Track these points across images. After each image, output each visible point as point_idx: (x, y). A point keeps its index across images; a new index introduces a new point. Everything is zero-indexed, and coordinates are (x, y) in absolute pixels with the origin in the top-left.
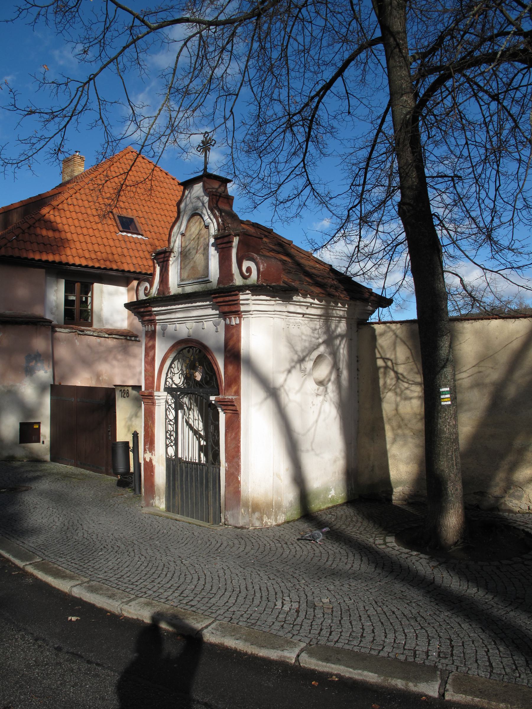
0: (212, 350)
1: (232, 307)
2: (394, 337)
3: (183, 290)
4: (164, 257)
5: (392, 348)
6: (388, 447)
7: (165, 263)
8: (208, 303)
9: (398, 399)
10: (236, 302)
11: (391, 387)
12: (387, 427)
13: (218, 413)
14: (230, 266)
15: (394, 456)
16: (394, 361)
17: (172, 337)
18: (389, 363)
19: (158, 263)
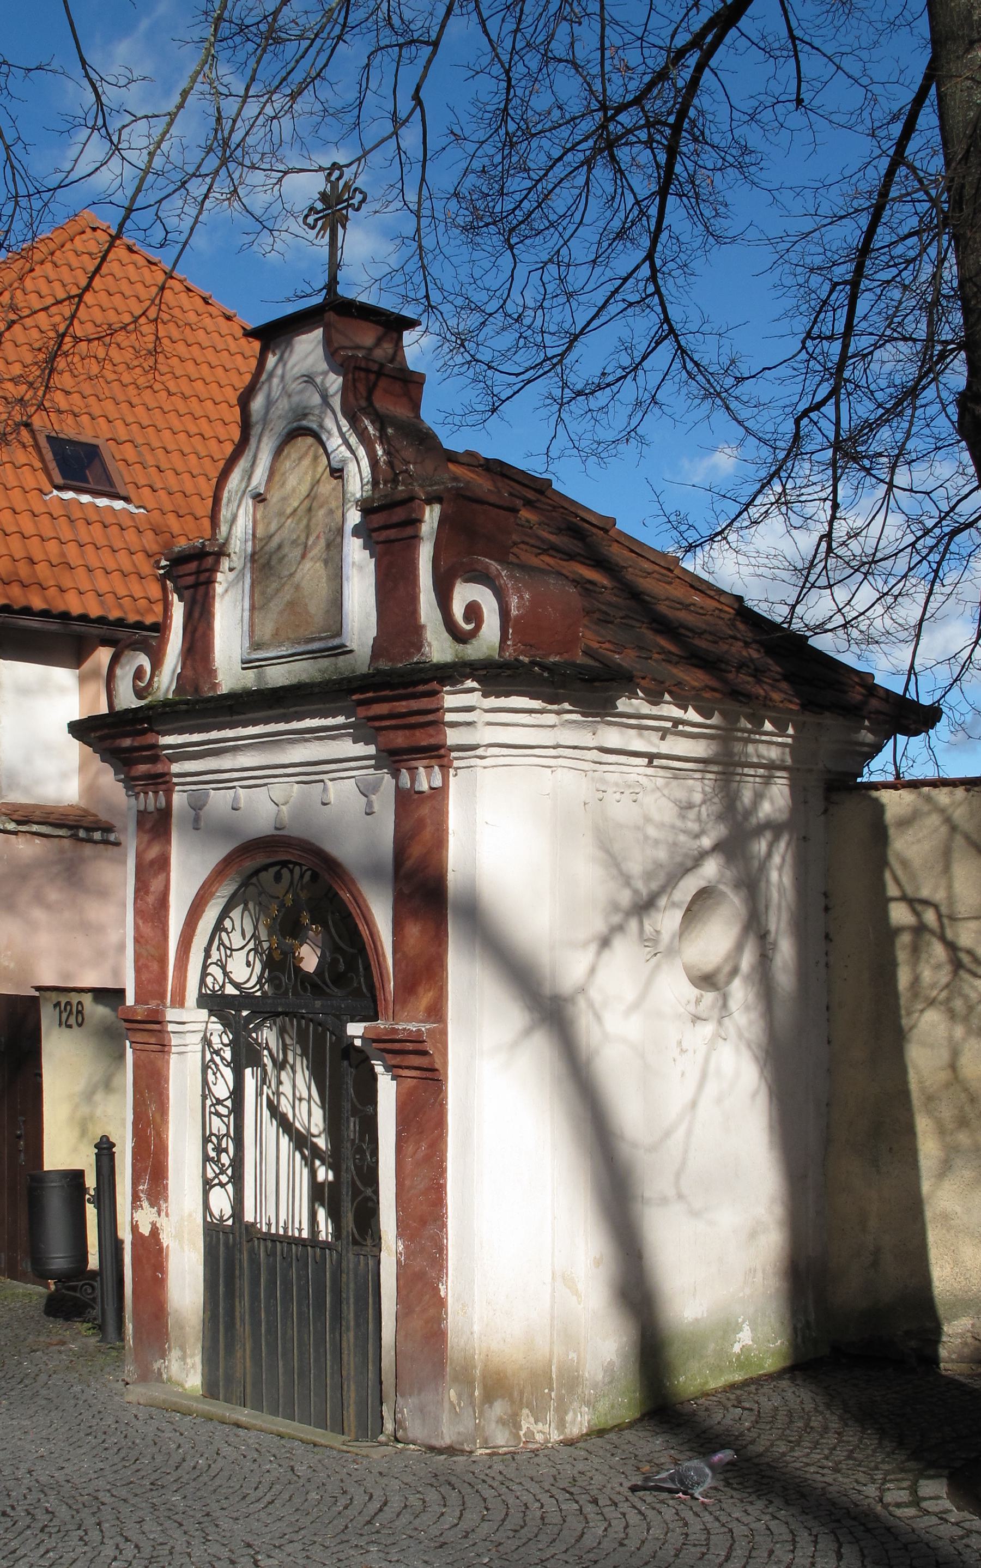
0: (354, 872)
1: (418, 733)
2: (944, 830)
3: (260, 677)
4: (198, 572)
5: (939, 868)
6: (926, 1186)
7: (202, 589)
8: (341, 720)
9: (959, 1031)
10: (430, 718)
11: (934, 993)
12: (923, 1124)
13: (374, 1078)
15: (945, 1217)
16: (944, 910)
17: (224, 830)
18: (930, 917)
19: (177, 590)
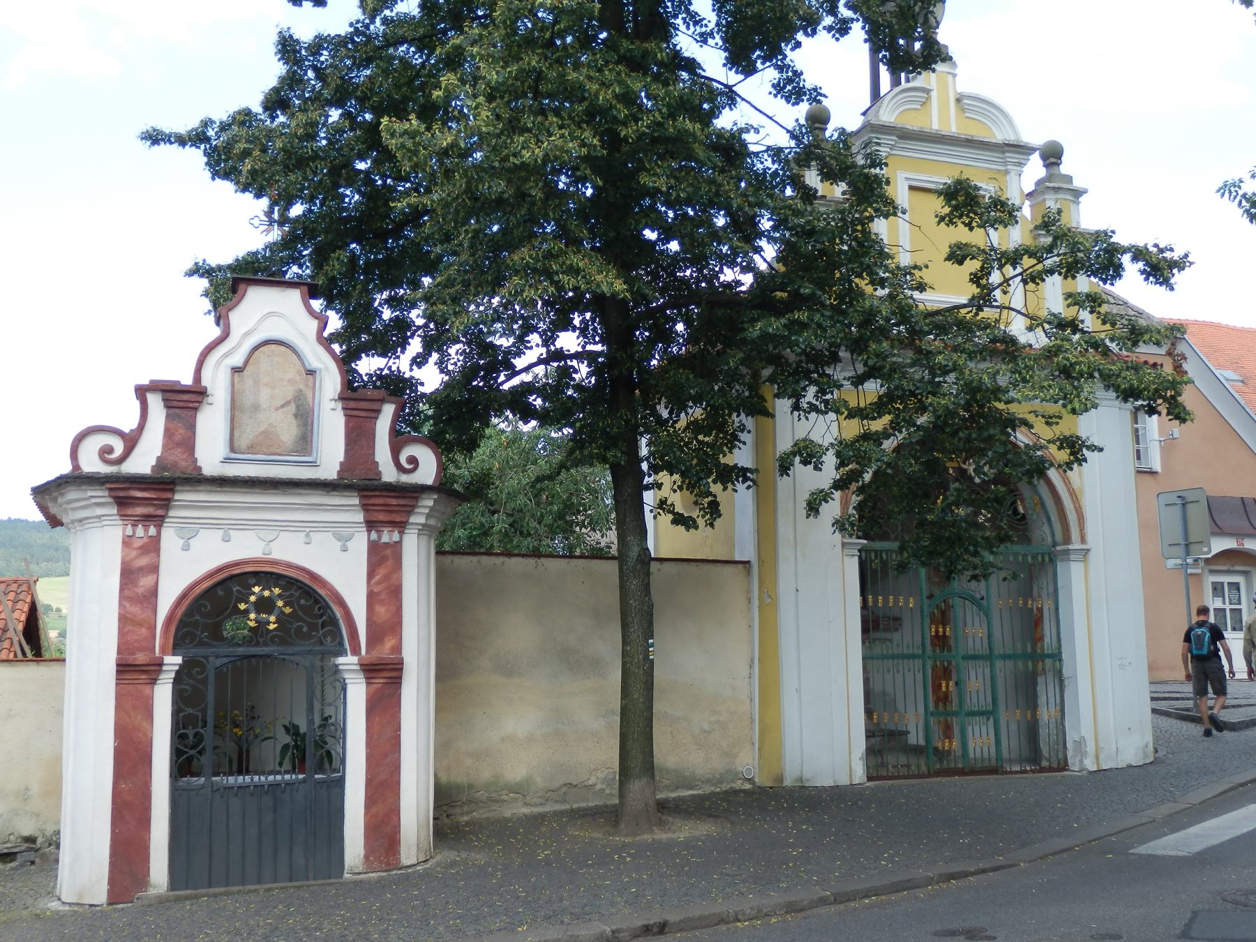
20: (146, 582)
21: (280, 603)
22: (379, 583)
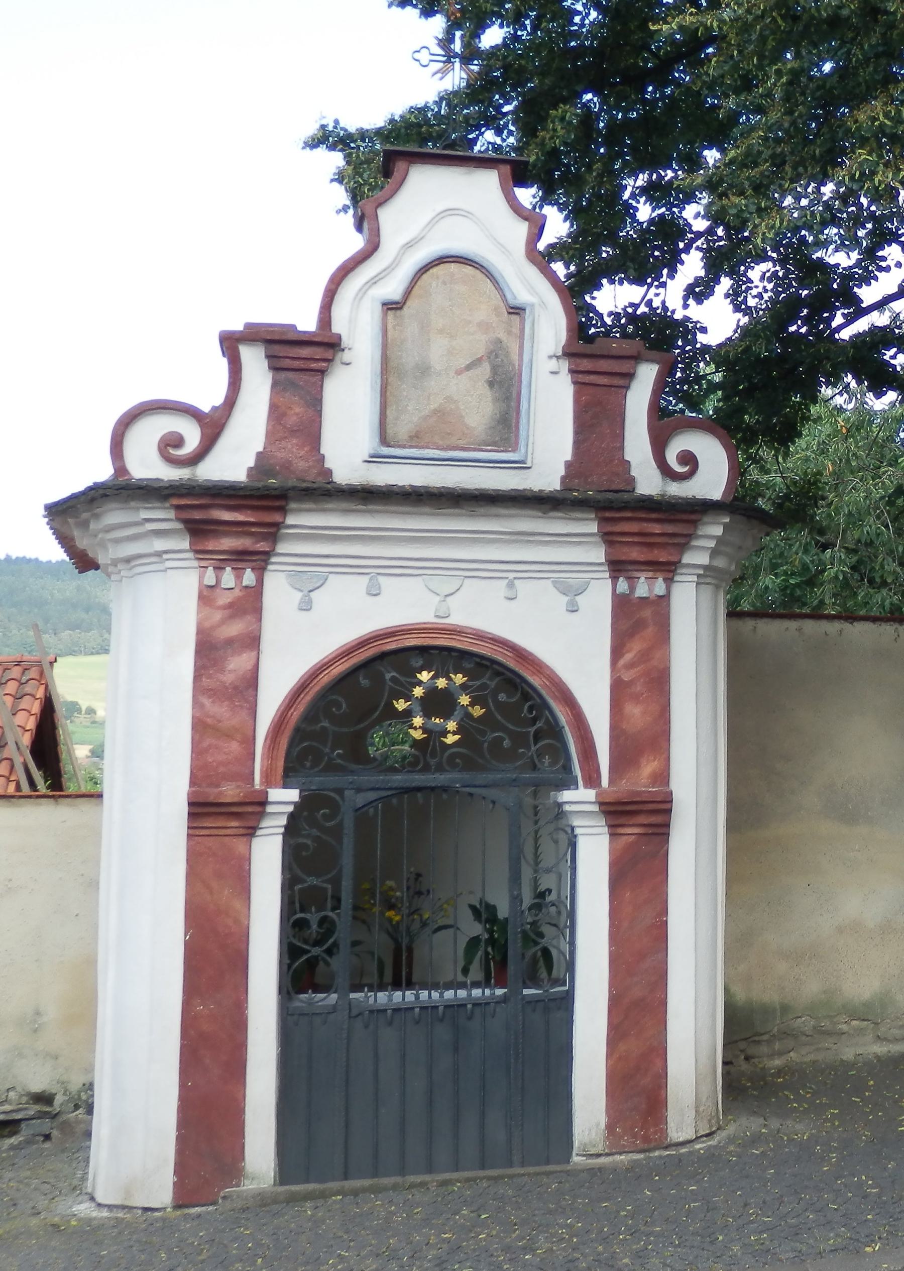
14: (619, 436)
20: (238, 663)
21: (464, 700)
22: (631, 666)
